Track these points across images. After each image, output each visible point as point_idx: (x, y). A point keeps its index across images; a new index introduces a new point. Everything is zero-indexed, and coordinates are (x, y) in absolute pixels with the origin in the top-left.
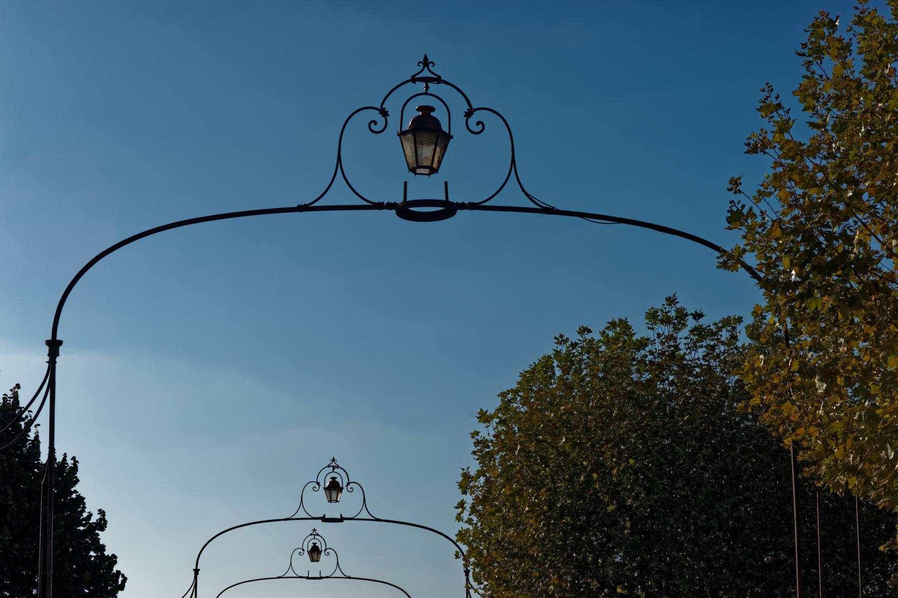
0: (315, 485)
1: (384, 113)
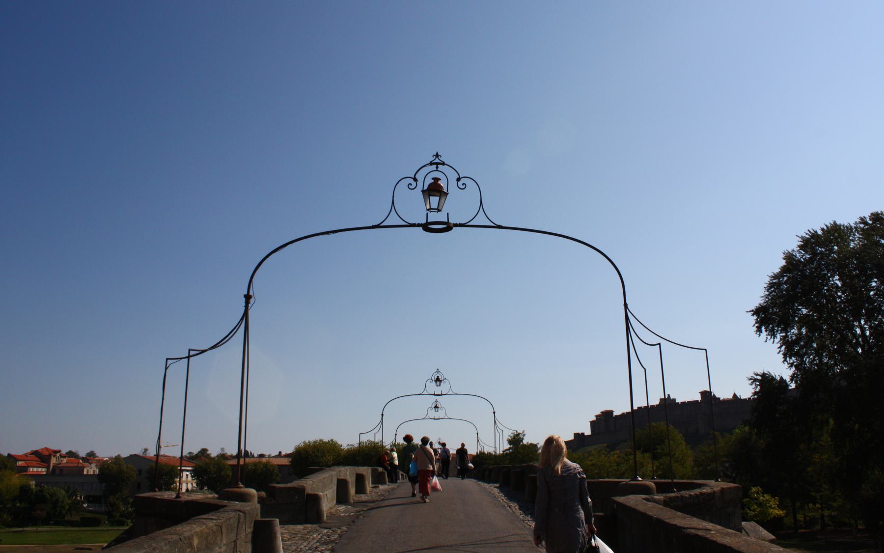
0: (412, 181)
1: (415, 180)
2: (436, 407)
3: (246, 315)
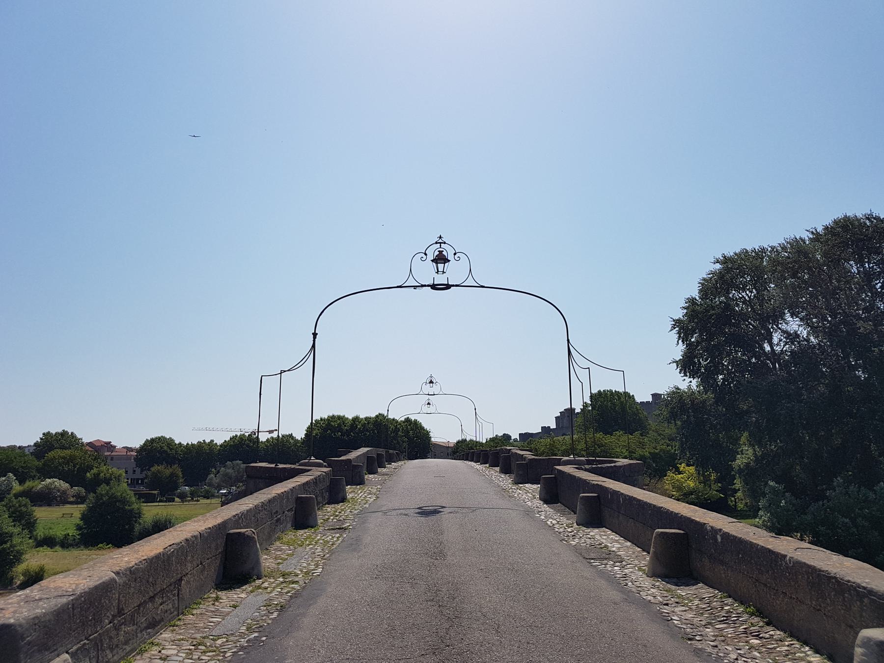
0: (423, 255)
1: (426, 254)
2: (431, 382)
3: (314, 346)
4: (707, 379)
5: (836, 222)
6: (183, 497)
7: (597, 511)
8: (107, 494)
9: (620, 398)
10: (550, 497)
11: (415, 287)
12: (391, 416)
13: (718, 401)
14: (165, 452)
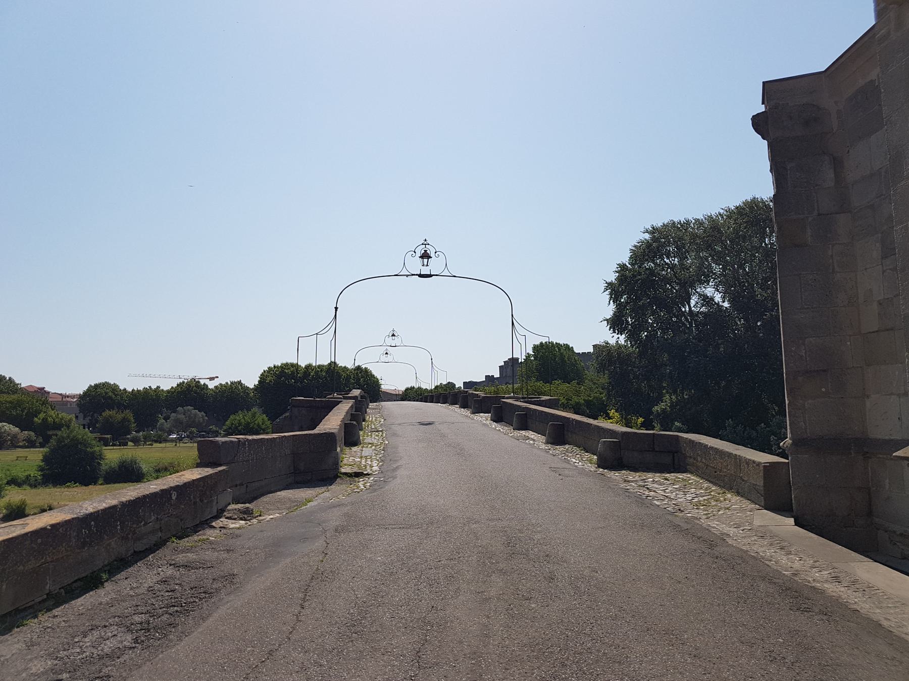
2: (393, 335)
4: (633, 336)
5: (746, 203)
6: (136, 441)
7: (524, 421)
8: (68, 437)
9: (559, 349)
10: (497, 419)
11: (407, 276)
12: (303, 364)
13: (641, 354)
14: (110, 398)
